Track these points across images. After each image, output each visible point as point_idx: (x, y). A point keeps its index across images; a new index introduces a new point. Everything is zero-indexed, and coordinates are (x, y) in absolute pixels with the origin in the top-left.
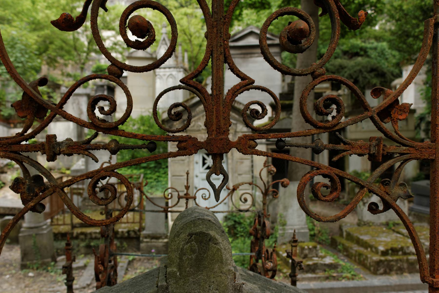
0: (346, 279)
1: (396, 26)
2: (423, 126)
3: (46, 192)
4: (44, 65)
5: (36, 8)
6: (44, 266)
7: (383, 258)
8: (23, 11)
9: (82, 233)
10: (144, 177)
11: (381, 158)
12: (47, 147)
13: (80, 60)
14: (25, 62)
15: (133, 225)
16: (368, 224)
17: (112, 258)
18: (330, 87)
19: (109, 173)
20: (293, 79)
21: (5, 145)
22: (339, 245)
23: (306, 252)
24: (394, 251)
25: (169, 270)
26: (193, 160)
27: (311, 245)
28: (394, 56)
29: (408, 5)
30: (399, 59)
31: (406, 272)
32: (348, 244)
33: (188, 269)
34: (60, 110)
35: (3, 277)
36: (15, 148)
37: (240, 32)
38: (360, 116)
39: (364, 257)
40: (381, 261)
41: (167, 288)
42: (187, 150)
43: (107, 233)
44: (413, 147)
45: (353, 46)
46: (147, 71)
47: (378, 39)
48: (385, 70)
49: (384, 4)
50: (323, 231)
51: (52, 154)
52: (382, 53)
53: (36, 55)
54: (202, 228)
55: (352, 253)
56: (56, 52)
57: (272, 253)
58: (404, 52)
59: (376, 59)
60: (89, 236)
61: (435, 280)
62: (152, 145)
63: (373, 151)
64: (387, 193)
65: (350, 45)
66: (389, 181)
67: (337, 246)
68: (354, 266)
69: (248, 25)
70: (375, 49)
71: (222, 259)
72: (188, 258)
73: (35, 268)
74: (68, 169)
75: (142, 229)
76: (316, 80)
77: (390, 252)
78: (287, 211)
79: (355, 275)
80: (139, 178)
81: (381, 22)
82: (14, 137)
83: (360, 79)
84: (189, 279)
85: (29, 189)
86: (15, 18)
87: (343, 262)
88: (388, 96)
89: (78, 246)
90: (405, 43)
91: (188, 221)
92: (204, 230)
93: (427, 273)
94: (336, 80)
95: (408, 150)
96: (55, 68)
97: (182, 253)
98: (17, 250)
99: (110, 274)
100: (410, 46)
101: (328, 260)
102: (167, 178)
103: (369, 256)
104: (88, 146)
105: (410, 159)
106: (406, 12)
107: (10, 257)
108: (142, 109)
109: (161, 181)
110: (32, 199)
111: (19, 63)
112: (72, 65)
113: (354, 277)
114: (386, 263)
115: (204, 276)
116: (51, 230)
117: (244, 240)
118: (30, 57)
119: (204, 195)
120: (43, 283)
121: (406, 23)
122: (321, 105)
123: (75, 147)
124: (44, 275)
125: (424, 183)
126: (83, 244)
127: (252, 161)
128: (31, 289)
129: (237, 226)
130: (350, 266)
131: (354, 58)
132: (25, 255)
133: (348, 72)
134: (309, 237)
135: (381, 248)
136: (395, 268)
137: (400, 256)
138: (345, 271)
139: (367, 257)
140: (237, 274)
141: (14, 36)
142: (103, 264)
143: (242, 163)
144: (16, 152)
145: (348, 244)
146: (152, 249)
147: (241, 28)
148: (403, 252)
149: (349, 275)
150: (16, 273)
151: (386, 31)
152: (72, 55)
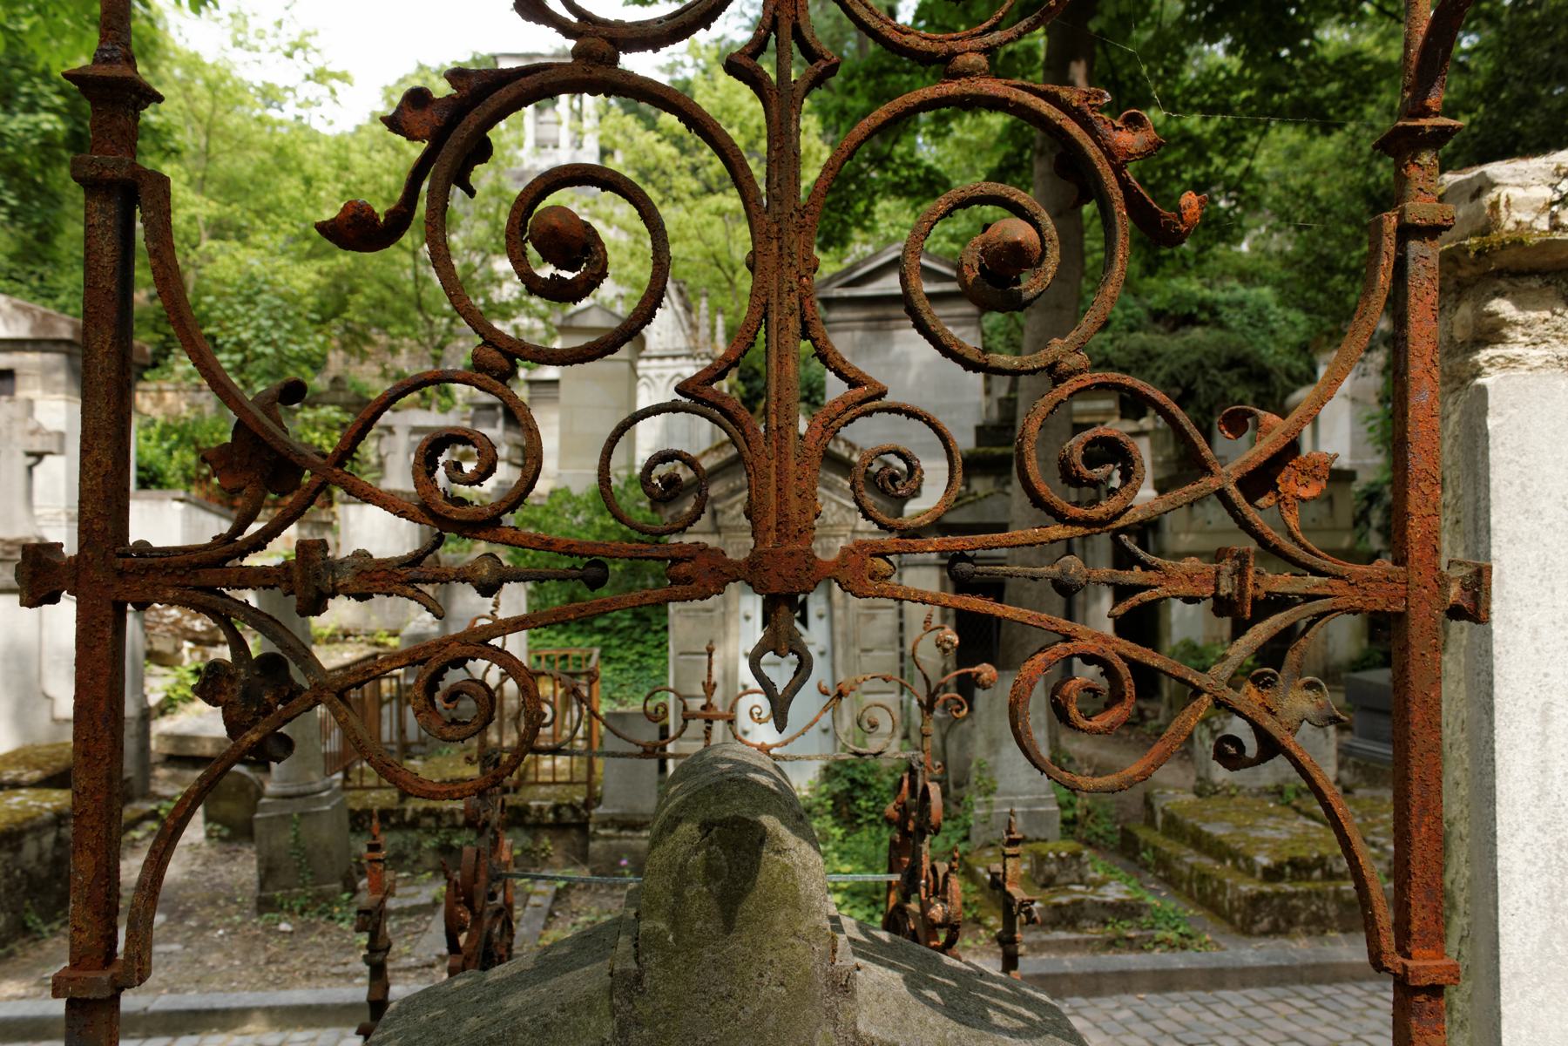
0: (1164, 947)
1: (1296, 243)
2: (1376, 517)
3: (295, 701)
4: (335, 349)
5: (315, 198)
6: (321, 904)
7: (1267, 889)
8: (279, 204)
9: (428, 812)
10: (601, 657)
11: (1249, 609)
12: (297, 577)
13: (431, 336)
14: (280, 343)
15: (568, 789)
16: (1228, 793)
17: (498, 886)
18: (1118, 411)
19: (472, 649)
20: (1013, 388)
21: (180, 568)
22: (1145, 850)
23: (1053, 868)
24: (1300, 868)
25: (645, 925)
26: (737, 610)
27: (1065, 848)
28: (1294, 324)
29: (1328, 184)
30: (1308, 333)
31: (1332, 929)
32: (1168, 846)
33: (699, 924)
34: (337, 471)
35: (209, 934)
36: (207, 577)
37: (867, 260)
38: (1187, 489)
39: (1215, 884)
40: (1262, 895)
41: (639, 979)
42: (695, 585)
43: (483, 816)
44: (1342, 578)
45: (1179, 298)
46: (582, 362)
47: (1247, 277)
48: (1269, 363)
49: (1264, 183)
50: (1100, 810)
51: (312, 594)
52: (1259, 318)
53: (312, 322)
54: (738, 807)
55: (1180, 872)
56: (368, 315)
57: (946, 876)
58: (1323, 314)
59: (1243, 332)
60: (447, 821)
61: (1409, 963)
62: (594, 571)
63: (1226, 588)
64: (1269, 710)
65: (1169, 295)
66: (1273, 675)
67: (1137, 853)
68: (1186, 911)
69: (889, 241)
70: (1241, 304)
71: (796, 897)
72: (699, 892)
73: (297, 909)
74: (395, 635)
75: (593, 800)
76: (1061, 386)
77: (1288, 870)
78: (997, 752)
79: (1189, 937)
80: (588, 659)
81: (1255, 232)
82: (206, 547)
83: (1201, 387)
84: (700, 954)
85: (246, 694)
86: (258, 223)
87: (1157, 899)
88: (1267, 432)
89: (418, 846)
90: (1322, 289)
91: (700, 787)
92: (745, 812)
93: (1388, 941)
94: (1133, 391)
95: (1327, 585)
96: (364, 357)
97: (682, 879)
98: (248, 858)
99: (490, 933)
100: (1339, 297)
101: (1113, 893)
102: (666, 658)
103: (1228, 881)
104: (414, 572)
105: (1333, 611)
106: (1323, 204)
107: (227, 878)
108: (565, 469)
109: (648, 668)
110: (255, 722)
111: (266, 344)
112: (411, 351)
113: (1189, 942)
114: (1276, 901)
115: (744, 945)
116: (343, 802)
117: (878, 833)
118: (294, 330)
119: (756, 710)
120: (317, 951)
121: (1326, 233)
122: (1077, 457)
123: (379, 576)
124: (323, 927)
125: (1381, 677)
126: (429, 843)
127: (901, 614)
128: (283, 967)
129: (858, 793)
130: (1174, 911)
131: (1181, 331)
132: (268, 872)
133: (1166, 369)
134: (1058, 825)
135: (1263, 860)
136: (1302, 917)
137: (1316, 882)
138: (1162, 925)
139: (1221, 883)
140: (842, 938)
141: (254, 270)
142: (469, 904)
143: (873, 617)
144: (211, 590)
145: (1168, 846)
146: (621, 858)
147: (870, 249)
148: (1323, 871)
149: (1173, 935)
150: (243, 923)
151: (1269, 258)
152: (412, 323)
